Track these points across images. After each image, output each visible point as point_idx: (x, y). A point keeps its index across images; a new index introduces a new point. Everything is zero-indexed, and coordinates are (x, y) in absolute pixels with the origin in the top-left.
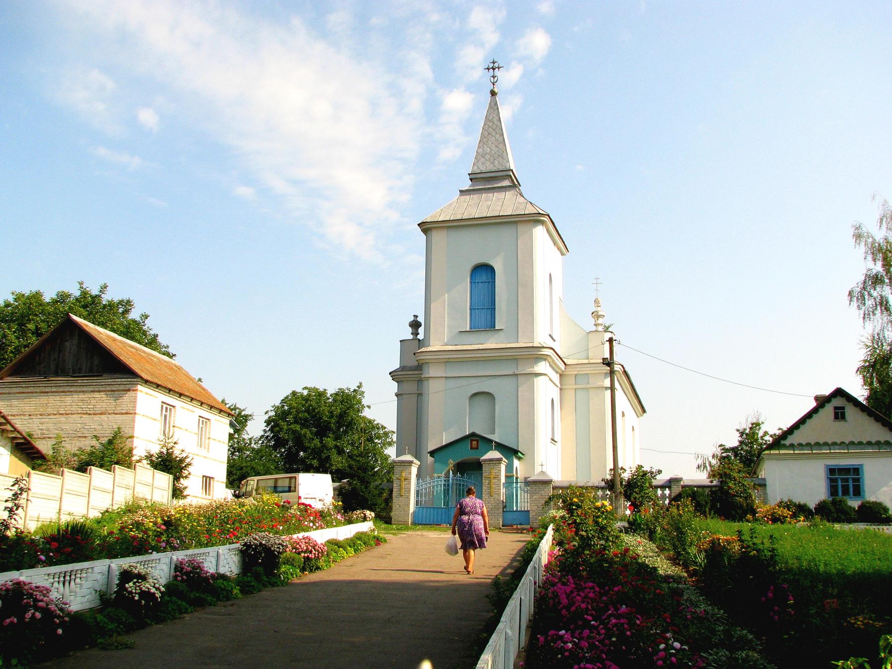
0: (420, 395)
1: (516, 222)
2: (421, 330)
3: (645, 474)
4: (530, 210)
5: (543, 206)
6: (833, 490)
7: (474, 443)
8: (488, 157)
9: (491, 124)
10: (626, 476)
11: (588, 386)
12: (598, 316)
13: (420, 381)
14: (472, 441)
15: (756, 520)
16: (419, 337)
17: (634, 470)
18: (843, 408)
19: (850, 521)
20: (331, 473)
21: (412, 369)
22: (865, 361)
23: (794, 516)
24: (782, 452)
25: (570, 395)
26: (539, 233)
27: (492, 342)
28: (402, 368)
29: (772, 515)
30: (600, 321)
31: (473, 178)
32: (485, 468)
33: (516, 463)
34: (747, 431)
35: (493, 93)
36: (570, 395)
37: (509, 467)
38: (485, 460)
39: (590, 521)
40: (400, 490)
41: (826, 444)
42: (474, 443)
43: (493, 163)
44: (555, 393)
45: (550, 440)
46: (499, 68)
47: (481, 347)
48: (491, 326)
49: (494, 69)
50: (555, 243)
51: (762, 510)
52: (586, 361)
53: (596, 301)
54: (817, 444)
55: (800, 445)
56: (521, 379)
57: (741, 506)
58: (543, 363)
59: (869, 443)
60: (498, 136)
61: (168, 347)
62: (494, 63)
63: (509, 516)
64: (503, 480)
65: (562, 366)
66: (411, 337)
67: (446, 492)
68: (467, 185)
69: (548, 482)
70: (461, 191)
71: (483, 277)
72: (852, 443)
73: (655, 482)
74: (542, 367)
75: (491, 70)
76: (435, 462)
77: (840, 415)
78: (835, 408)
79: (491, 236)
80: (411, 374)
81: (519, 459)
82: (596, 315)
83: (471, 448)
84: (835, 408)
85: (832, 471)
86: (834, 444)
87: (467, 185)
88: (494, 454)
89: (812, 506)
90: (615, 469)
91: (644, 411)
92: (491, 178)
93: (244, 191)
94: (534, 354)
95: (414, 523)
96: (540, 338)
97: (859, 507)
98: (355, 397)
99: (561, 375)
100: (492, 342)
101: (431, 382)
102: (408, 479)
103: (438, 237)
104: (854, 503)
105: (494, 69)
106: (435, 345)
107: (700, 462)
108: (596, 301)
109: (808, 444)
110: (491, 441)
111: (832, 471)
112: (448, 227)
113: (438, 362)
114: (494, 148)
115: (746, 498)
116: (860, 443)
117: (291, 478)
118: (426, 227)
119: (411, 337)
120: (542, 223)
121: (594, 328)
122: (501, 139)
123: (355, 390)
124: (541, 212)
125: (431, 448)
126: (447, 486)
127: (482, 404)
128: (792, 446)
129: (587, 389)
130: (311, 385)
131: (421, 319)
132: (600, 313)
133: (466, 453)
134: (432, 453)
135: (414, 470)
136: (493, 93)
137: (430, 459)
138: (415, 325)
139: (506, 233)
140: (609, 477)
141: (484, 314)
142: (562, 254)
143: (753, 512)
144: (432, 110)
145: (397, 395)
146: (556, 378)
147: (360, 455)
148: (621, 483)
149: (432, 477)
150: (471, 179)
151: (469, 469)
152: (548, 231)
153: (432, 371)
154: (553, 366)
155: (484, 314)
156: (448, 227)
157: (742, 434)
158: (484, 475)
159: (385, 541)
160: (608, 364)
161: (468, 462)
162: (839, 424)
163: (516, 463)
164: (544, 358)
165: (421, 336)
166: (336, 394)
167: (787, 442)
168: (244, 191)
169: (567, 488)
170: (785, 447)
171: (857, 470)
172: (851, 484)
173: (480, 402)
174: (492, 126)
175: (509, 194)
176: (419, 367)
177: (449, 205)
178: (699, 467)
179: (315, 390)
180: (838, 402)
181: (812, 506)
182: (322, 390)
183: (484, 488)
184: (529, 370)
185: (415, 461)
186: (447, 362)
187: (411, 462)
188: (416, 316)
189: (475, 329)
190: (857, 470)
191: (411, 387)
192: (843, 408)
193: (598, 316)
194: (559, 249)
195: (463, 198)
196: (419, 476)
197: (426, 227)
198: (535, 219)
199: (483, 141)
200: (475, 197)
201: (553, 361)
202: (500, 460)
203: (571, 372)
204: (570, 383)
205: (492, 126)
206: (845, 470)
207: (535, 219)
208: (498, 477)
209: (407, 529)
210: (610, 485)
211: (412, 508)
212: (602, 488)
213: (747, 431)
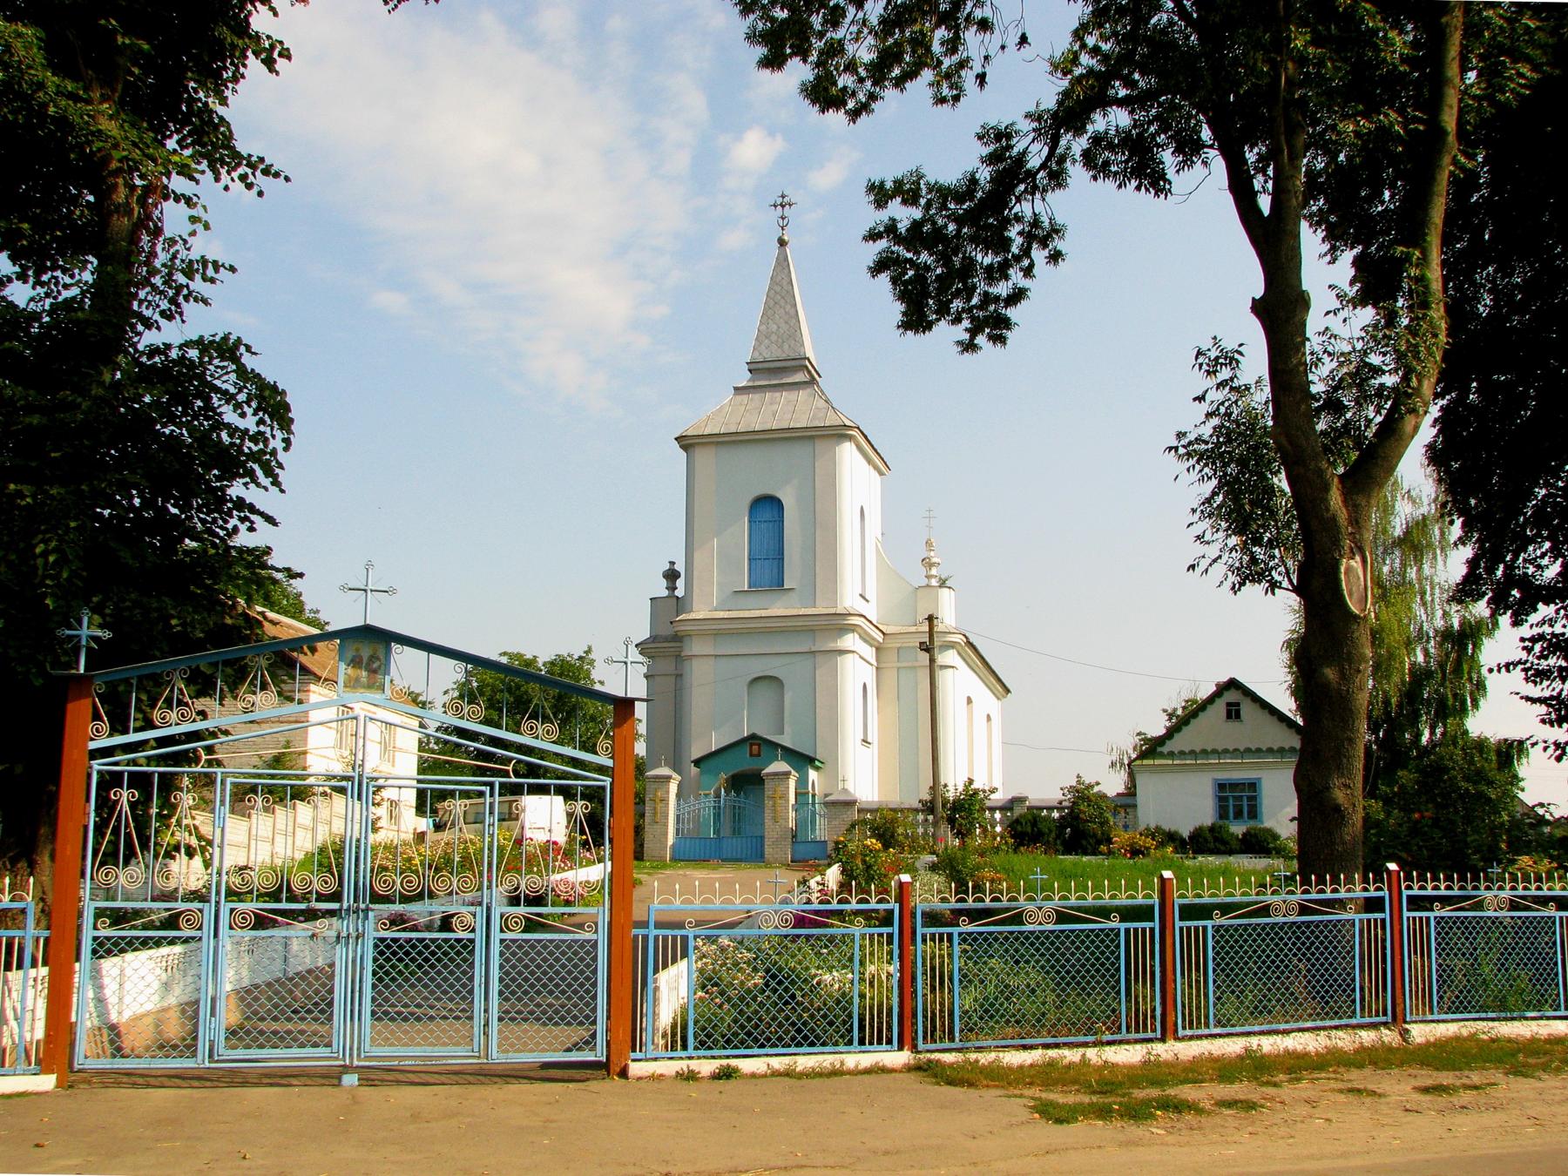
0: (679, 676)
1: (812, 438)
2: (680, 583)
3: (976, 792)
4: (831, 420)
5: (848, 411)
6: (1223, 813)
7: (755, 748)
8: (774, 338)
9: (778, 289)
10: (951, 795)
12: (931, 565)
13: (679, 658)
15: (1110, 853)
16: (677, 593)
17: (961, 788)
18: (1238, 704)
19: (1231, 852)
20: (121, 249)
21: (666, 639)
22: (1294, 631)
23: (1161, 845)
24: (1157, 762)
25: (890, 677)
26: (847, 454)
27: (779, 607)
28: (654, 638)
29: (1131, 845)
30: (934, 571)
31: (755, 368)
32: (768, 785)
33: (813, 775)
34: (1179, 712)
36: (890, 677)
37: (802, 782)
38: (768, 774)
39: (859, 862)
40: (655, 814)
41: (1214, 751)
42: (755, 748)
43: (781, 347)
44: (868, 675)
47: (763, 613)
48: (778, 584)
49: (783, 206)
50: (869, 461)
51: (1120, 838)
52: (913, 629)
53: (928, 543)
54: (1204, 752)
55: (1182, 753)
56: (820, 658)
57: (1095, 836)
58: (850, 636)
59: (1270, 750)
60: (788, 307)
61: (318, 611)
62: (783, 197)
63: (801, 847)
64: (792, 800)
65: (879, 637)
66: (665, 593)
67: (717, 816)
68: (744, 379)
69: (850, 804)
70: (736, 389)
71: (767, 513)
72: (1248, 750)
73: (988, 803)
74: (850, 641)
76: (702, 773)
77: (1233, 713)
78: (1229, 704)
79: (778, 456)
80: (667, 645)
81: (817, 769)
82: (928, 563)
84: (1229, 704)
85: (1221, 786)
86: (1226, 751)
87: (744, 379)
88: (780, 766)
89: (1186, 834)
90: (933, 788)
91: (1008, 691)
92: (779, 369)
93: (390, 301)
94: (838, 623)
95: (673, 859)
96: (849, 599)
97: (1244, 835)
98: (581, 667)
99: (878, 649)
100: (779, 607)
101: (695, 662)
102: (665, 800)
103: (703, 456)
104: (1238, 829)
105: (783, 206)
106: (700, 611)
107: (1115, 757)
108: (928, 543)
109: (1192, 752)
110: (776, 745)
111: (1221, 786)
113: (703, 634)
114: (783, 325)
115: (1102, 824)
116: (1259, 750)
117: (511, 802)
118: (687, 443)
119: (665, 593)
120: (850, 438)
121: (924, 582)
122: (792, 312)
123: (580, 658)
124: (848, 423)
125: (695, 756)
126: (717, 808)
127: (765, 693)
128: (1171, 755)
129: (914, 667)
130: (513, 649)
131: (680, 567)
132: (934, 560)
134: (697, 762)
135: (673, 787)
136: (782, 243)
137: (694, 770)
139: (800, 451)
140: (927, 797)
141: (769, 566)
142: (881, 473)
143: (1109, 841)
144: (707, 168)
145: (646, 676)
146: (869, 653)
148: (944, 806)
149: (697, 796)
151: (747, 783)
152: (859, 447)
153: (696, 647)
154: (866, 639)
155: (769, 566)
157: (1171, 716)
158: (767, 793)
159: (159, 328)
160: (927, 650)
161: (745, 773)
162: (1233, 725)
163: (813, 775)
164: (853, 628)
165: (680, 592)
166: (552, 663)
167: (1165, 749)
168: (390, 301)
169: (877, 810)
170: (1162, 755)
171: (1253, 786)
172: (1245, 802)
173: (764, 691)
174: (780, 295)
175: (803, 394)
176: (677, 638)
177: (715, 403)
178: (1113, 765)
179: (519, 656)
180: (1231, 696)
181: (1186, 834)
182: (529, 656)
183: (767, 811)
184: (831, 646)
185: (675, 775)
187: (669, 777)
188: (672, 563)
190: (1253, 786)
191: (667, 666)
192: (1238, 704)
193: (931, 565)
194: (876, 468)
195: (739, 398)
196: (678, 796)
197: (687, 443)
198: (840, 433)
200: (756, 397)
202: (788, 774)
203: (893, 644)
204: (891, 659)
205: (780, 295)
206: (1234, 786)
207: (840, 433)
208: (785, 797)
209: (665, 867)
210: (929, 807)
211: (670, 841)
212: (917, 811)
213: (1179, 712)
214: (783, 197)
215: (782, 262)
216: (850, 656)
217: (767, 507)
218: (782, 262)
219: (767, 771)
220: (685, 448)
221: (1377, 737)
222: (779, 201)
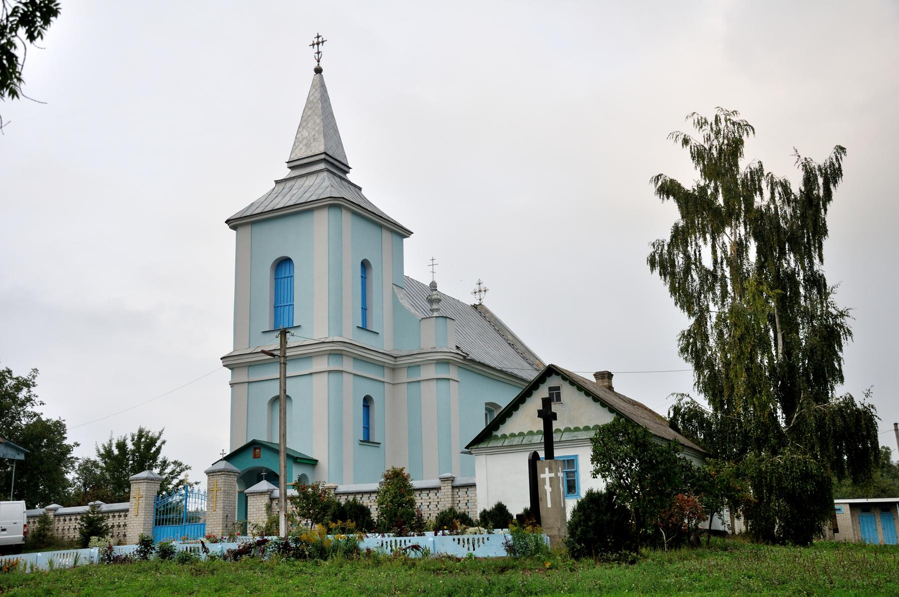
11: (419, 379)
14: (255, 449)
35: (318, 71)
46: (323, 42)
62: (318, 37)
68: (286, 173)
75: (316, 46)
87: (286, 173)
105: (318, 44)
174: (320, 106)
197: (234, 223)
205: (320, 106)
220: (234, 228)
222: (316, 41)
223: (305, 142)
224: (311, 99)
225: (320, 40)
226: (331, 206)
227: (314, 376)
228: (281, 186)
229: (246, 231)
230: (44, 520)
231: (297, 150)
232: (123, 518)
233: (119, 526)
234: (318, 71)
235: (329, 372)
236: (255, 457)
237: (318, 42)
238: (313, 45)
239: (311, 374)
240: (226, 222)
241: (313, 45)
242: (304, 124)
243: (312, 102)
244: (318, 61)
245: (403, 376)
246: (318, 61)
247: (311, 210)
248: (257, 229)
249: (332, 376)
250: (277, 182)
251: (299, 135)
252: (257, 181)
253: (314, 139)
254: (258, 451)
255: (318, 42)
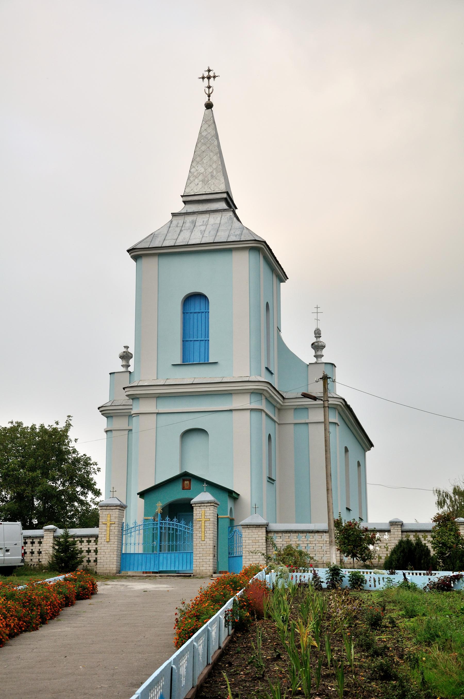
11: (307, 421)
14: (184, 481)
35: (209, 106)
45: (265, 479)
46: (214, 77)
53: (318, 334)
62: (209, 71)
65: (279, 400)
68: (180, 207)
75: (206, 80)
82: (318, 347)
83: (183, 489)
87: (180, 207)
105: (209, 78)
112: (184, 576)
129: (307, 424)
131: (131, 350)
133: (176, 494)
138: (126, 357)
147: (385, 654)
150: (185, 202)
156: (184, 576)
174: (209, 143)
186: (159, 397)
188: (127, 347)
189: (186, 362)
197: (136, 253)
199: (197, 158)
201: (271, 396)
205: (209, 143)
214: (209, 71)
215: (210, 123)
216: (288, 426)
217: (195, 301)
218: (210, 123)
219: (196, 499)
220: (135, 258)
221: (68, 504)
222: (206, 74)
223: (201, 178)
224: (204, 134)
225: (211, 74)
226: (252, 249)
227: (234, 412)
228: (180, 220)
229: (151, 264)
230: (66, 536)
231: (192, 185)
232: (36, 544)
233: (32, 553)
234: (209, 106)
235: (252, 410)
236: (183, 489)
237: (209, 76)
238: (203, 78)
239: (231, 410)
240: (128, 251)
241: (203, 78)
242: (198, 159)
243: (205, 137)
244: (209, 96)
245: (290, 417)
246: (209, 96)
247: (230, 250)
248: (167, 263)
249: (254, 414)
250: (174, 215)
251: (193, 170)
252: (155, 213)
253: (212, 176)
254: (186, 482)
255: (209, 76)
